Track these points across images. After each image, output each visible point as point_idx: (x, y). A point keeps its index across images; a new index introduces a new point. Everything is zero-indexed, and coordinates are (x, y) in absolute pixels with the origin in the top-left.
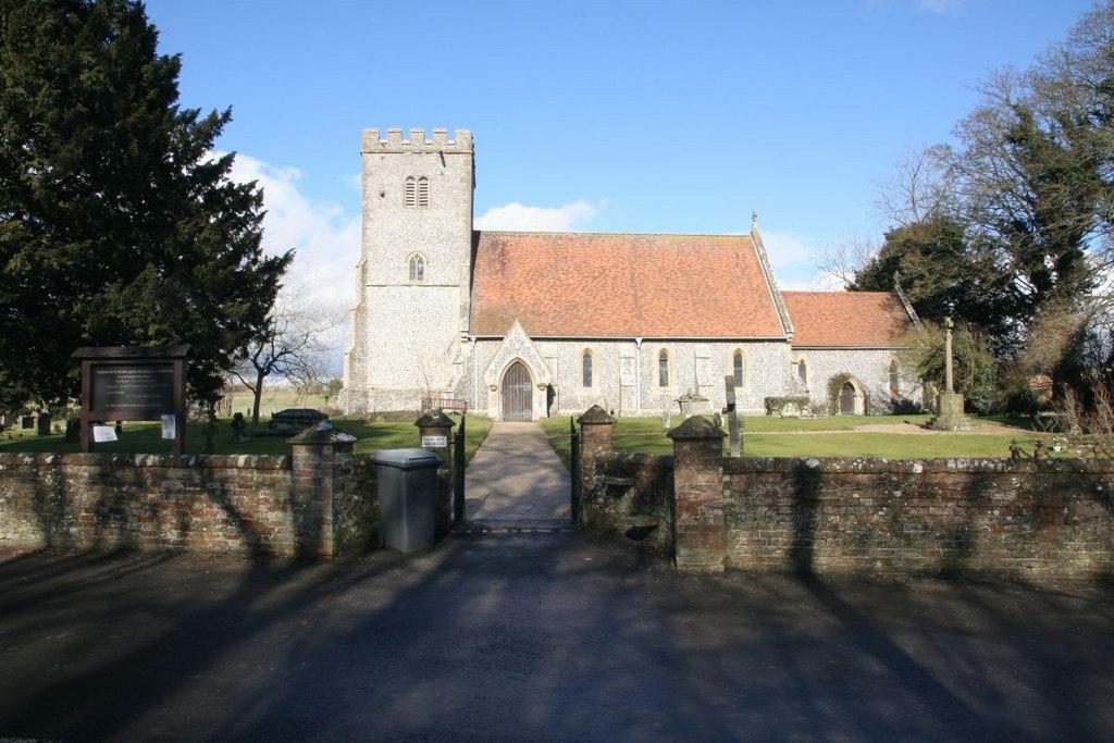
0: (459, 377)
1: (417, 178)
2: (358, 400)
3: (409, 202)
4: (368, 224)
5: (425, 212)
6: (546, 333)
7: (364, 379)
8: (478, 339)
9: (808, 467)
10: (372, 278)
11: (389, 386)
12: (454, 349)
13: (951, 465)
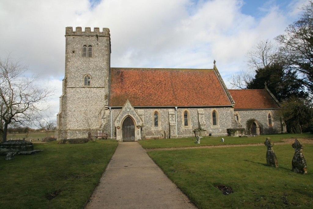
0: (104, 124)
4: (68, 63)
8: (112, 108)
10: (69, 84)
11: (76, 128)
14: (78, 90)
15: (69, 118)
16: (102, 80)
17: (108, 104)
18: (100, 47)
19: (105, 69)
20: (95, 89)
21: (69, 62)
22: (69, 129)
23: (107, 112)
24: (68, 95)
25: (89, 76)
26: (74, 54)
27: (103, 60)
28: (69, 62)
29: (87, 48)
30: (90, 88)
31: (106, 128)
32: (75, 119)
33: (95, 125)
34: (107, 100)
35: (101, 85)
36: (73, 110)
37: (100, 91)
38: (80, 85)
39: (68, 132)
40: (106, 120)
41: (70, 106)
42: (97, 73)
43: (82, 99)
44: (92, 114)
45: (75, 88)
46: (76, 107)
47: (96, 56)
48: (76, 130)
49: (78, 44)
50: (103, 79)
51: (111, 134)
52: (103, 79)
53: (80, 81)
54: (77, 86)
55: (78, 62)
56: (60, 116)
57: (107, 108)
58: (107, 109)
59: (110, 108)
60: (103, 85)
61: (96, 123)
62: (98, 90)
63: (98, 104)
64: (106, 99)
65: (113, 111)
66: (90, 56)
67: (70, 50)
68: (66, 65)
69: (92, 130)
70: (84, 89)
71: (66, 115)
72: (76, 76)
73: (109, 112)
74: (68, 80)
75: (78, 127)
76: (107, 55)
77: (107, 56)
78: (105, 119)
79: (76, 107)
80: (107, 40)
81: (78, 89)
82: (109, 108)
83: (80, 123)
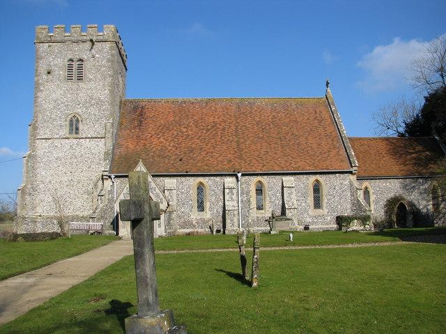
2: (27, 224)
3: (70, 78)
5: (81, 84)
6: (305, 196)
7: (34, 208)
8: (116, 177)
14: (57, 143)
16: (101, 123)
25: (77, 116)
29: (75, 65)
42: (93, 110)
54: (56, 136)
59: (113, 177)
62: (93, 142)
65: (118, 181)
66: (80, 78)
70: (67, 141)
72: (53, 116)
80: (111, 48)
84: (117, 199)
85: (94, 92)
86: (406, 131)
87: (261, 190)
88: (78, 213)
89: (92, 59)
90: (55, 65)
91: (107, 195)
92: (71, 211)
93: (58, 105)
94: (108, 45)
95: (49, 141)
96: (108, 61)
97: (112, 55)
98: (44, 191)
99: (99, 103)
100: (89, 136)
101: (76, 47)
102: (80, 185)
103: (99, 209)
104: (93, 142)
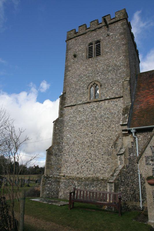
0: (121, 167)
1: (94, 43)
2: (51, 184)
3: (90, 56)
4: (68, 73)
5: (99, 58)
6: (117, 94)
7: (59, 169)
8: (138, 131)
9: (23, 90)
10: (68, 102)
11: (74, 174)
12: (119, 142)
13: (110, 188)
14: (80, 108)
15: (66, 157)
16: (118, 85)
17: (126, 123)
18: (112, 38)
19: (122, 67)
20: (107, 101)
21: (69, 71)
22: (64, 176)
23: (127, 141)
24: (66, 117)
25: (97, 83)
26: (76, 59)
27: (119, 54)
28: (69, 71)
29: (94, 47)
30: (98, 102)
31: (126, 178)
32: (74, 159)
33: (109, 170)
34: (126, 115)
35: (117, 94)
36: (71, 142)
37: (116, 103)
38: (83, 100)
39: (62, 180)
40: (123, 159)
41: (67, 135)
42: (110, 76)
43: (85, 122)
44: (102, 147)
45: (75, 106)
46: (76, 137)
47: (107, 52)
48: (74, 179)
49: (81, 45)
50: (120, 82)
51: (139, 194)
52: (120, 82)
53: (84, 93)
54: (79, 103)
55: (83, 68)
56: (49, 152)
57: (126, 130)
58: (125, 135)
59: (133, 131)
60: (120, 93)
61: (110, 166)
62: (112, 102)
63: (113, 128)
64: (123, 114)
65: (140, 137)
66: (98, 54)
67: (71, 54)
68: (66, 76)
69: (102, 180)
70: (88, 105)
71: (60, 150)
72: (78, 87)
73: (132, 140)
74: (67, 96)
75: (78, 173)
76: (123, 45)
77: (124, 46)
78: (123, 157)
79: (76, 137)
80: (122, 25)
81: (80, 106)
82: (130, 132)
83: (82, 166)
84: (141, 155)
85: (111, 60)
86: (147, 224)
87: (73, 208)
88: (98, 175)
89: (107, 38)
90: (79, 51)
91: (127, 154)
92: (91, 172)
93: (81, 78)
94: (119, 24)
95: (75, 107)
96: (121, 34)
97: (124, 29)
98: (69, 152)
99: (116, 68)
100: (108, 97)
101: (94, 34)
102: (100, 145)
103: (118, 172)
104: (112, 103)
